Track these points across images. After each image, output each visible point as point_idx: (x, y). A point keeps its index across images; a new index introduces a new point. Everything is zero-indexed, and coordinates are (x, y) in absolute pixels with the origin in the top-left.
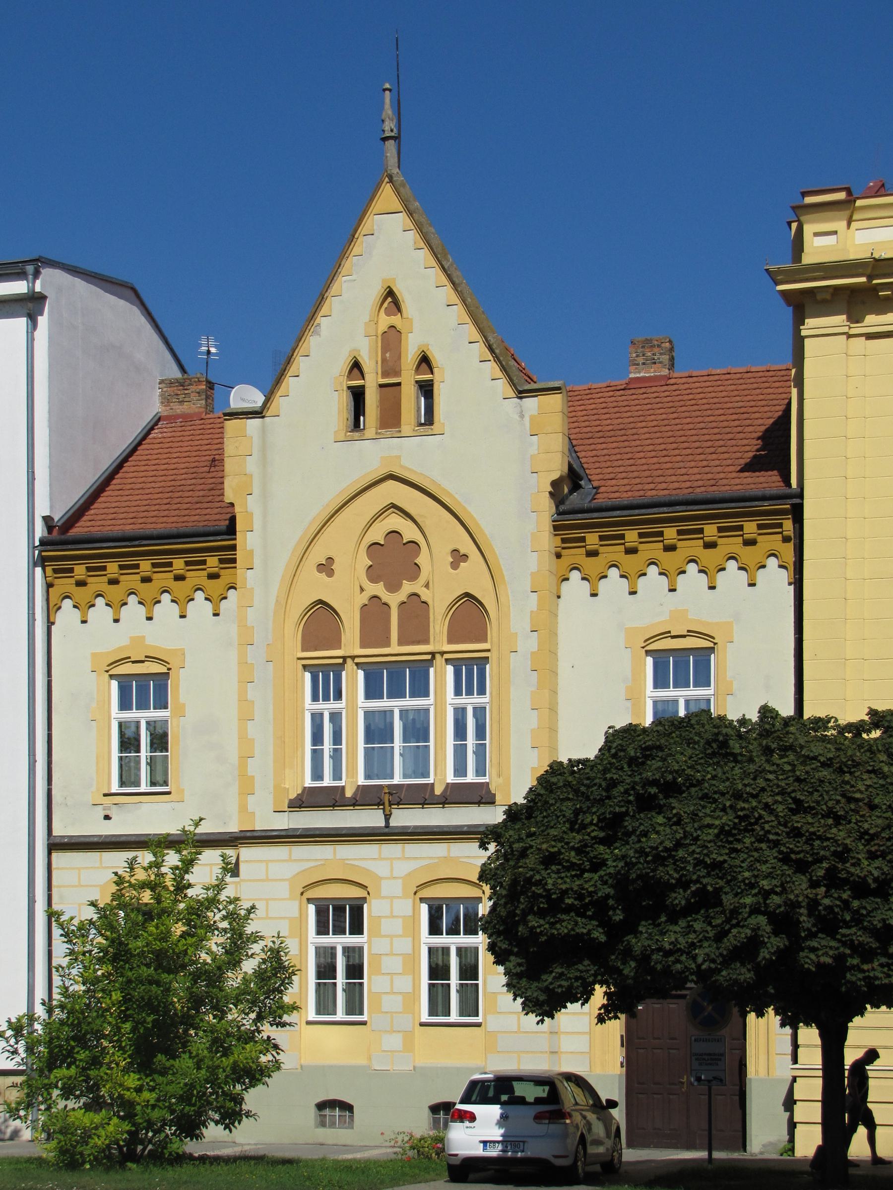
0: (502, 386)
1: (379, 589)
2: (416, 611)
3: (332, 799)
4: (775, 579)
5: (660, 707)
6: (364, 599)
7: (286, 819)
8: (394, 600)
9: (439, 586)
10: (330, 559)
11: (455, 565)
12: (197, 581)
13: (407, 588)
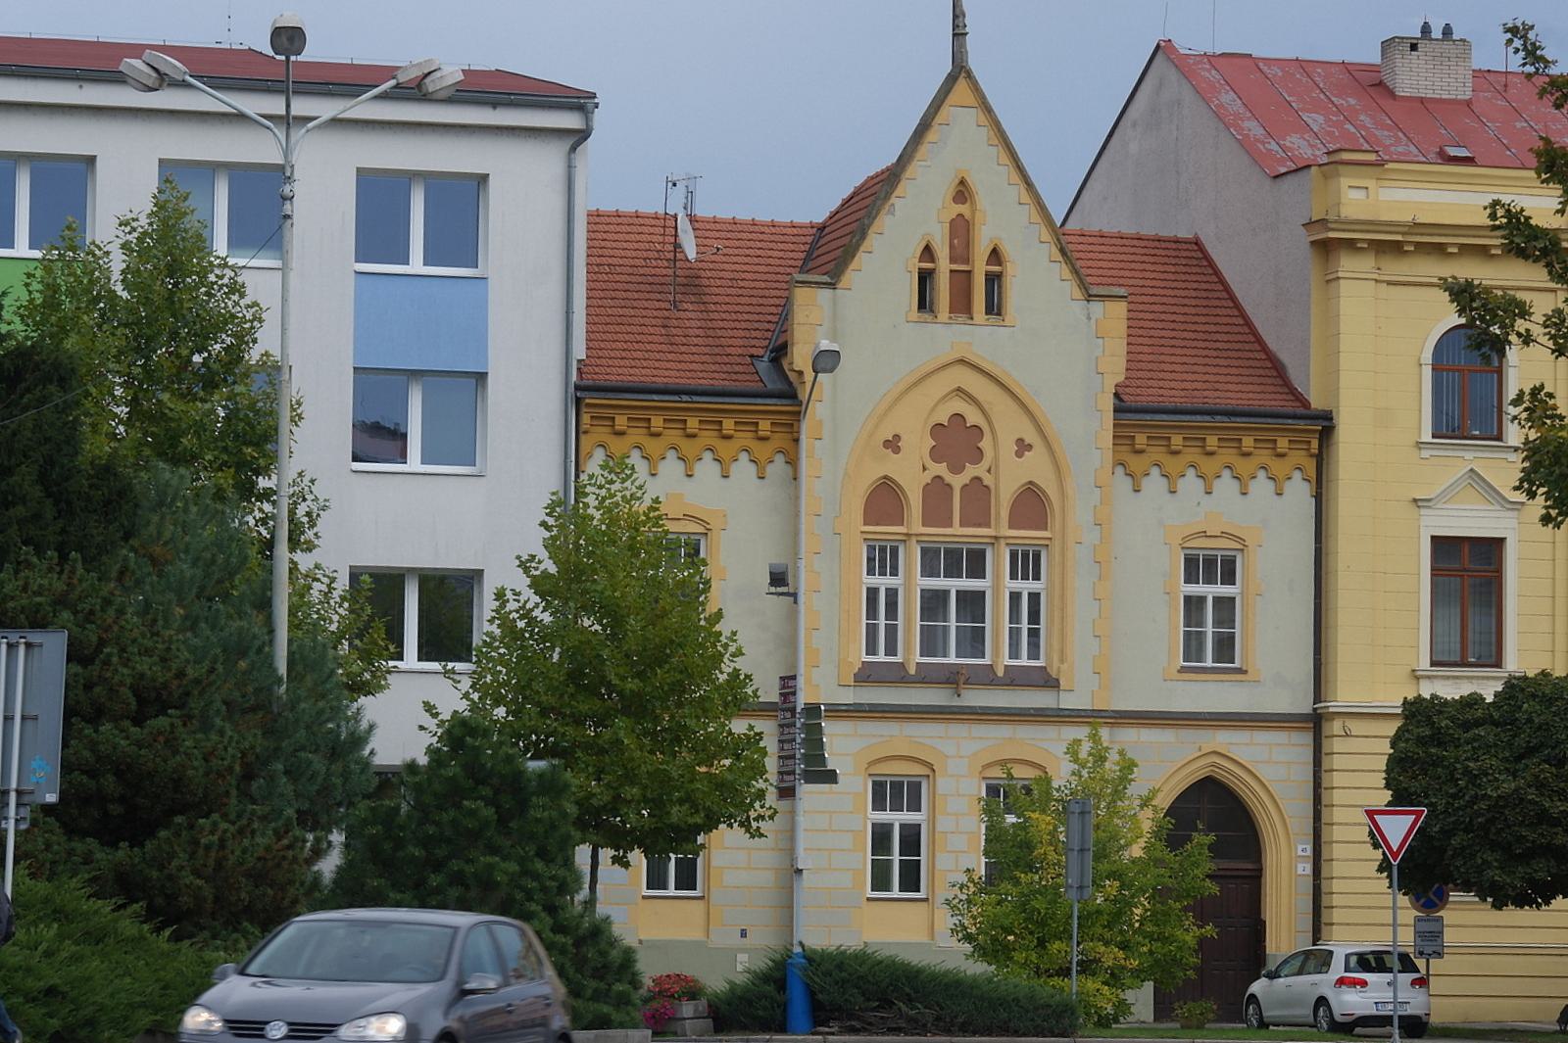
0: (1071, 288)
1: (941, 469)
2: (978, 492)
3: (897, 676)
4: (1299, 491)
5: (927, 595)
6: (927, 477)
7: (852, 695)
8: (957, 481)
9: (1008, 477)
10: (897, 437)
11: (1019, 454)
12: (745, 443)
13: (971, 471)
